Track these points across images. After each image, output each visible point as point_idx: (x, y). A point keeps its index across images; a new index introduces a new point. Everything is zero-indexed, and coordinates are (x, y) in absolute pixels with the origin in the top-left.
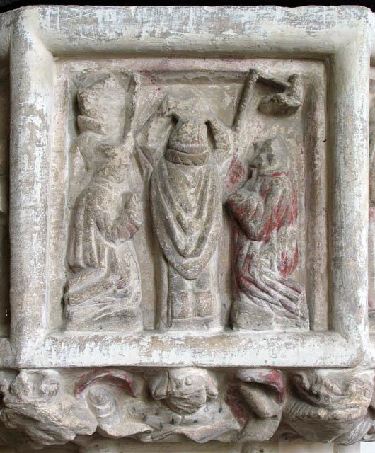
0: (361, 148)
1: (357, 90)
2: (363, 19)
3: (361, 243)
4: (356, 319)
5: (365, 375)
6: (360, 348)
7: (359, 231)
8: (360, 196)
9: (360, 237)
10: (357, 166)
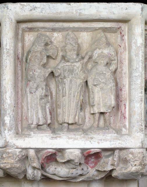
0: (6, 60)
1: (4, 38)
2: (6, 8)
3: (6, 98)
4: (4, 129)
5: (15, 151)
6: (5, 140)
7: (5, 94)
8: (5, 79)
9: (6, 96)
10: (4, 68)
